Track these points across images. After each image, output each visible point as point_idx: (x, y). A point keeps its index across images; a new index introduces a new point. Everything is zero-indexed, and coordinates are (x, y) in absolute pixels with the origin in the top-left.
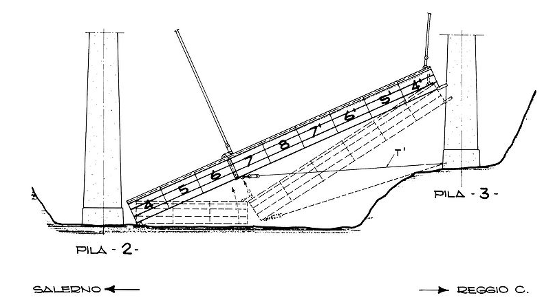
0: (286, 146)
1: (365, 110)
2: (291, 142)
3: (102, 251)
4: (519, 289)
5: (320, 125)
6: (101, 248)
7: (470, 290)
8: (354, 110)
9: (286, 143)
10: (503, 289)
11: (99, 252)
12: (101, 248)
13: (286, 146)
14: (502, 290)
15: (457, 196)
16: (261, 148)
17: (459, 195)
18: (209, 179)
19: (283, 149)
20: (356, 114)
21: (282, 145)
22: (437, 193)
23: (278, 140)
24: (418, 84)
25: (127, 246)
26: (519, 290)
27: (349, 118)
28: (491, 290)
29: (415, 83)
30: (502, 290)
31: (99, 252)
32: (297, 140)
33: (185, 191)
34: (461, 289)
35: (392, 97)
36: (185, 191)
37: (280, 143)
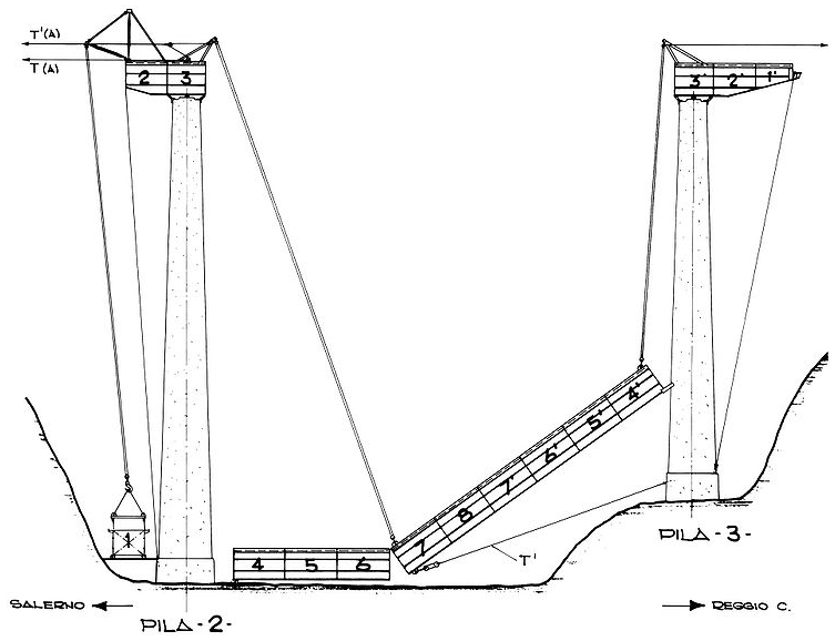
0: (469, 516)
1: (568, 443)
2: (473, 510)
3: (700, 536)
4: (782, 606)
5: (512, 477)
6: (700, 532)
7: (726, 606)
8: (555, 446)
9: (467, 513)
10: (762, 606)
11: (696, 538)
12: (700, 532)
13: (469, 516)
14: (763, 606)
15: (178, 630)
16: (479, 495)
17: (183, 627)
18: (626, 401)
19: (465, 522)
20: (557, 452)
21: (462, 517)
22: (664, 533)
23: (456, 511)
24: (636, 391)
25: (217, 620)
26: (781, 606)
27: (550, 457)
28: (750, 607)
29: (631, 390)
30: (763, 606)
31: (696, 538)
32: (483, 504)
33: (596, 424)
34: (717, 605)
35: (602, 418)
36: (596, 424)
37: (459, 514)
